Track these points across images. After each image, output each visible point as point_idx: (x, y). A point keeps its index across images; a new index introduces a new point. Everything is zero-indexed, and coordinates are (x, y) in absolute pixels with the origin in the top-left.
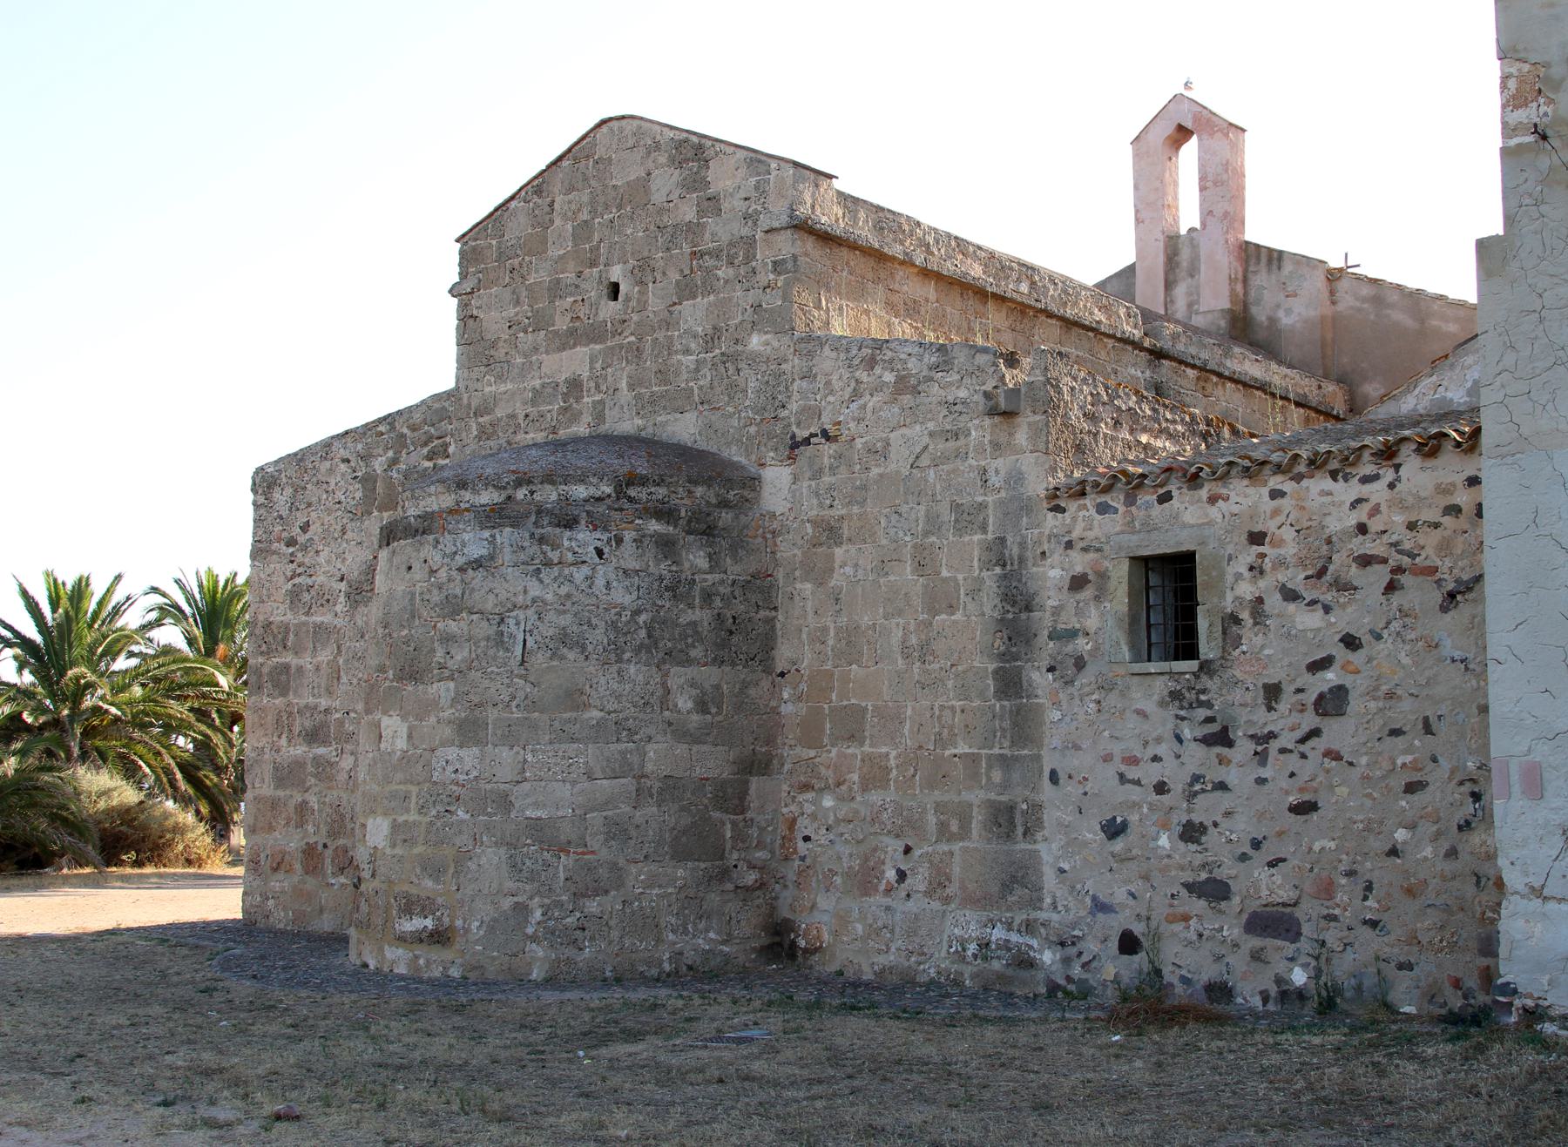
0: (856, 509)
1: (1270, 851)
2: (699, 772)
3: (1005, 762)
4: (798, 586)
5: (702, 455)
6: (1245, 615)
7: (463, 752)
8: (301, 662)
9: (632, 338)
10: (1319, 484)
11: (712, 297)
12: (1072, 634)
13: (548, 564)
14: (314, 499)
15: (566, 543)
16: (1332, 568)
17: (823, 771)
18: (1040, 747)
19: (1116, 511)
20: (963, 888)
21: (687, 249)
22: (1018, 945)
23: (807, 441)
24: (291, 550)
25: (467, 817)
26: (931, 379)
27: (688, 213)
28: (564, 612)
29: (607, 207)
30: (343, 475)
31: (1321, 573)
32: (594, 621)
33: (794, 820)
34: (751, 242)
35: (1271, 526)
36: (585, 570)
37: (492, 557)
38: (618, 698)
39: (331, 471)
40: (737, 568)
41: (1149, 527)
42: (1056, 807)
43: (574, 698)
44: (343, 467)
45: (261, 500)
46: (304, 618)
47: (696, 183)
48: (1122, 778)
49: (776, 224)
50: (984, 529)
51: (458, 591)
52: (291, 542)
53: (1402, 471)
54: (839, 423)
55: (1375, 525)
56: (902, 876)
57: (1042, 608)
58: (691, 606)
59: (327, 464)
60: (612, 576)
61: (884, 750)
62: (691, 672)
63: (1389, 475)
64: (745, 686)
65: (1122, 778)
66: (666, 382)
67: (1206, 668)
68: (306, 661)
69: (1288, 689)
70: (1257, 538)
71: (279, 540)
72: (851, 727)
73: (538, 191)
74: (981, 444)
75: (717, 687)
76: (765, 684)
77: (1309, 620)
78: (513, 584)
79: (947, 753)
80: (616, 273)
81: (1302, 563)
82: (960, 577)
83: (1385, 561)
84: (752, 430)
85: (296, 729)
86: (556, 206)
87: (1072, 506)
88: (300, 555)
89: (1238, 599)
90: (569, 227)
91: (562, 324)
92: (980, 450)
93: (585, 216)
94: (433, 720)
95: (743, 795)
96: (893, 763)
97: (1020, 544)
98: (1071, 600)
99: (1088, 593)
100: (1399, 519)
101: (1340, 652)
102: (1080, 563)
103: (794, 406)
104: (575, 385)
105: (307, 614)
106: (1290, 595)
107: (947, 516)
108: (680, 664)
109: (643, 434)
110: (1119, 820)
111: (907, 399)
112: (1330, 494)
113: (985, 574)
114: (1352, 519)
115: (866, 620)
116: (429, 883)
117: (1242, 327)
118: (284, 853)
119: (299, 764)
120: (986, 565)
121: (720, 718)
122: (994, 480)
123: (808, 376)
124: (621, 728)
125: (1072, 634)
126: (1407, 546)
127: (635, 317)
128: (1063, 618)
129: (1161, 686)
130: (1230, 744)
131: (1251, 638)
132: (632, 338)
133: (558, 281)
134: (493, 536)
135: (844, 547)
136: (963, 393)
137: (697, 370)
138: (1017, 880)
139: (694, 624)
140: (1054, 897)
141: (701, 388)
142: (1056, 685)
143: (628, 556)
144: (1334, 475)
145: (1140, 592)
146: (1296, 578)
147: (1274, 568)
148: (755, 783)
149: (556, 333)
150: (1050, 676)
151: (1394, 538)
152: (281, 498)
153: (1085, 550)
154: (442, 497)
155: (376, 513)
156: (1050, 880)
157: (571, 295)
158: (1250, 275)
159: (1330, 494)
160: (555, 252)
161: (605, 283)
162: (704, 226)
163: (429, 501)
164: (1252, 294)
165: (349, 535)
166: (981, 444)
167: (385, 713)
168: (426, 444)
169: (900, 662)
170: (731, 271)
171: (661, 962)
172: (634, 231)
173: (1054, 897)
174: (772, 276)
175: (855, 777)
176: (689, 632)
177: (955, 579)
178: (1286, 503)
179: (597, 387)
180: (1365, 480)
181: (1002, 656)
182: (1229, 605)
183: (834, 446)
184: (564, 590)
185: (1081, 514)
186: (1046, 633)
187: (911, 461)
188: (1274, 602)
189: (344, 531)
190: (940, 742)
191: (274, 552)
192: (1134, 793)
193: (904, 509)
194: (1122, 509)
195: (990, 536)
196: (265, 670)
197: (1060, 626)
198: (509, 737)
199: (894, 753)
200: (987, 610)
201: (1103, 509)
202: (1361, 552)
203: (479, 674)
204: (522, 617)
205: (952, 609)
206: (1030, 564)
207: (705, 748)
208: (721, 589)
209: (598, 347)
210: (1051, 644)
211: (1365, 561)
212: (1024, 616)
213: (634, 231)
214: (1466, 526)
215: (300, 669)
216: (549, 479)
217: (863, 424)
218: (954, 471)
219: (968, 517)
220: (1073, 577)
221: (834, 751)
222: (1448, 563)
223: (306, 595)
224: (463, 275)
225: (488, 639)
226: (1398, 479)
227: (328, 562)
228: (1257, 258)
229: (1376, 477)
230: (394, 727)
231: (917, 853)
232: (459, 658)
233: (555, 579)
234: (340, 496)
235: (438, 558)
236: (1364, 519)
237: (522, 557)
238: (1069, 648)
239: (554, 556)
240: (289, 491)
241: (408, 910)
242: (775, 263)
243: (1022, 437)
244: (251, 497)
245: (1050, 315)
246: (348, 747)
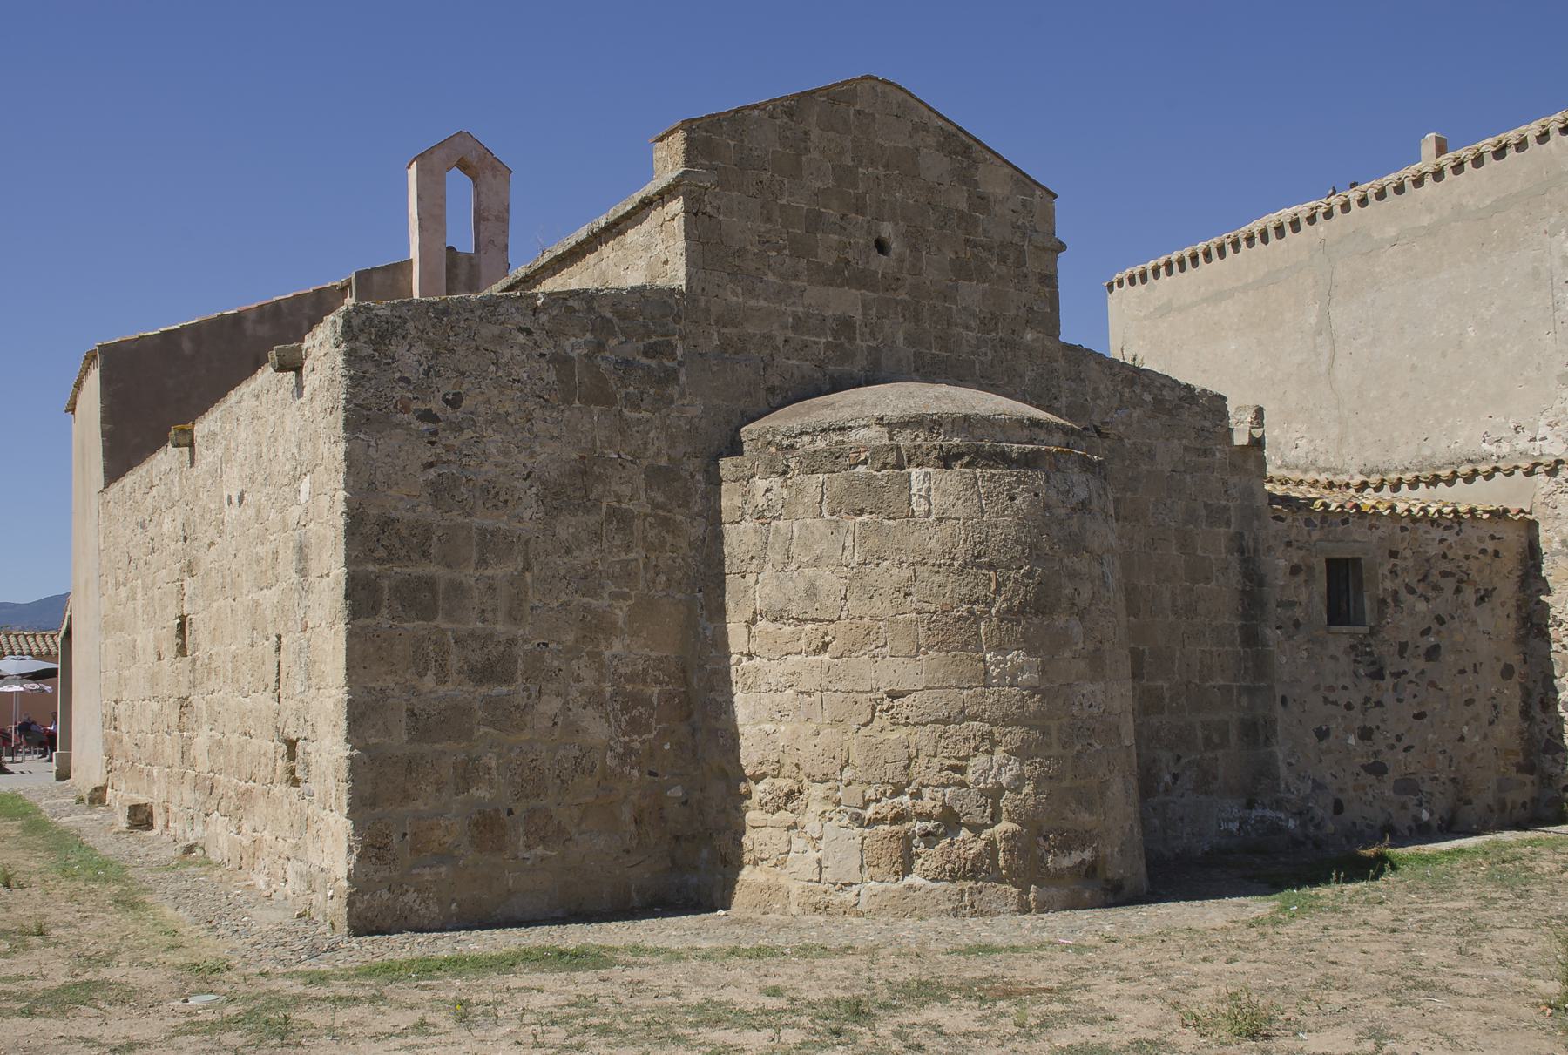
1: (1406, 741)
47: (965, 178)
48: (1326, 701)
50: (1228, 524)
56: (1175, 777)
65: (1326, 701)
69: (1411, 646)
73: (790, 112)
77: (1421, 606)
80: (887, 230)
83: (1453, 575)
99: (1301, 578)
101: (1435, 626)
106: (1412, 591)
116: (1086, 816)
129: (1345, 642)
130: (1383, 678)
141: (982, 363)
146: (1412, 579)
149: (820, 266)
156: (1283, 770)
188: (1403, 594)
191: (398, 426)
195: (1232, 530)
205: (1208, 580)
211: (1445, 574)
215: (457, 588)
231: (1184, 761)
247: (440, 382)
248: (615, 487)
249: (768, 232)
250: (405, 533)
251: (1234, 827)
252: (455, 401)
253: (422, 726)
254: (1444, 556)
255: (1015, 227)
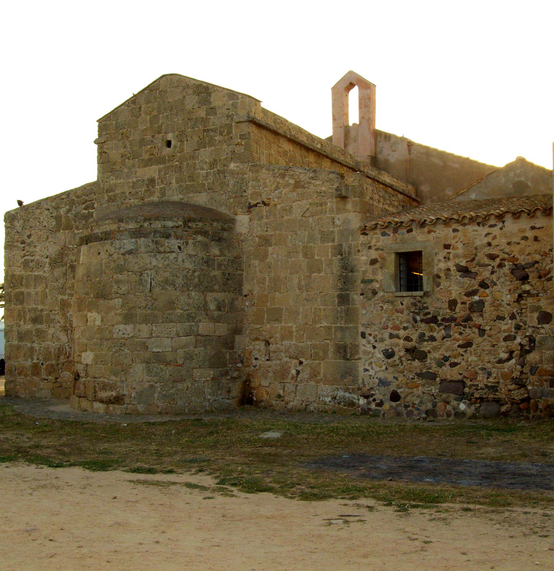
0: (278, 232)
2: (217, 333)
3: (342, 329)
4: (253, 262)
5: (211, 210)
6: (442, 275)
7: (127, 326)
8: (29, 290)
9: (177, 163)
10: (471, 228)
11: (213, 148)
12: (371, 281)
13: (160, 252)
14: (34, 225)
15: (166, 244)
16: (477, 258)
17: (264, 333)
18: (357, 323)
19: (389, 235)
20: (325, 376)
21: (201, 128)
22: (349, 398)
23: (256, 205)
24: (23, 245)
25: (129, 352)
26: (310, 183)
27: (202, 113)
28: (167, 271)
29: (165, 110)
30: (46, 215)
31: (473, 260)
32: (178, 275)
33: (251, 352)
34: (230, 126)
35: (453, 242)
36: (174, 255)
37: (137, 249)
38: (189, 305)
39: (41, 213)
40: (230, 255)
41: (403, 241)
42: (364, 345)
43: (171, 305)
44: (46, 212)
45: (9, 225)
46: (30, 273)
49: (242, 120)
50: (333, 241)
51: (122, 263)
52: (23, 242)
53: (505, 224)
54: (270, 199)
55: (494, 243)
56: (298, 372)
57: (358, 271)
58: (214, 269)
59: (39, 211)
60: (185, 257)
61: (291, 325)
62: (215, 295)
63: (500, 225)
64: (233, 300)
66: (194, 181)
67: (426, 294)
68: (32, 290)
70: (447, 247)
71: (17, 242)
72: (276, 315)
74: (332, 208)
75: (224, 301)
76: (240, 299)
78: (146, 260)
79: (317, 326)
80: (170, 137)
81: (465, 256)
82: (323, 259)
84: (232, 200)
85: (28, 317)
86: (142, 109)
87: (371, 233)
88: (27, 248)
89: (440, 270)
90: (148, 117)
91: (146, 157)
92: (332, 210)
93: (155, 113)
94: (113, 314)
95: (233, 342)
96: (294, 329)
97: (349, 247)
98: (370, 268)
99: (377, 265)
100: (504, 241)
102: (374, 254)
103: (249, 192)
104: (152, 181)
105: (32, 271)
107: (318, 236)
108: (210, 291)
109: (183, 201)
110: (390, 350)
111: (300, 190)
112: (477, 231)
113: (334, 258)
114: (486, 240)
115: (282, 275)
117: (375, 161)
118: (23, 367)
119: (28, 332)
120: (334, 255)
121: (224, 313)
122: (338, 222)
123: (256, 179)
124: (190, 318)
125: (371, 281)
126: (507, 250)
127: (179, 155)
128: (367, 275)
131: (444, 283)
132: (177, 163)
133: (144, 139)
134: (137, 241)
135: (272, 247)
136: (324, 189)
137: (207, 176)
138: (349, 373)
139: (214, 276)
140: (363, 380)
141: (208, 183)
142: (364, 300)
143: (190, 249)
144: (479, 224)
145: (398, 265)
147: (454, 257)
148: (237, 338)
149: (143, 160)
150: (362, 297)
151: (503, 247)
152: (18, 225)
153: (377, 249)
154: (111, 225)
155: (62, 231)
157: (149, 145)
158: (378, 142)
159: (477, 231)
160: (142, 127)
161: (165, 140)
162: (209, 119)
163: (105, 227)
164: (378, 150)
165: (50, 239)
166: (332, 208)
167: (90, 311)
168: (84, 203)
169: (297, 291)
170: (221, 137)
171: (206, 406)
172: (178, 120)
173: (363, 380)
174: (239, 140)
175: (278, 335)
176: (214, 279)
177: (321, 261)
178: (459, 234)
179: (162, 181)
180: (491, 226)
181: (341, 289)
182: (435, 271)
183: (268, 208)
184: (166, 263)
185: (375, 236)
186: (360, 280)
187: (302, 214)
189: (48, 238)
190: (315, 322)
191: (16, 246)
192: (396, 340)
193: (299, 232)
194: (392, 235)
195: (336, 244)
196: (12, 294)
197: (366, 278)
198: (146, 320)
199: (295, 326)
200: (335, 272)
201: (384, 234)
202: (489, 253)
203: (132, 296)
204: (149, 273)
205: (319, 271)
206: (353, 255)
207: (220, 324)
208: (224, 263)
209: (162, 166)
210: (362, 285)
212: (350, 274)
213: (178, 120)
214: (529, 244)
215: (29, 294)
216: (157, 219)
217: (280, 199)
218: (320, 218)
219: (326, 237)
220: (371, 260)
221: (268, 326)
222: (522, 257)
223: (31, 263)
224: (100, 135)
225: (136, 282)
226: (504, 226)
227: (41, 250)
228: (377, 134)
229: (495, 225)
230: (95, 318)
232: (124, 289)
233: (163, 258)
234: (45, 223)
235: (113, 250)
236: (490, 240)
237: (149, 250)
238: (370, 286)
239: (162, 249)
240: (21, 222)
241: (104, 387)
242: (241, 135)
243: (349, 206)
244: (4, 224)
245: (327, 157)
246: (51, 325)
247: (26, 231)
248: (70, 257)
249: (125, 151)
250: (17, 278)
251: (328, 399)
252: (29, 236)
253: (21, 337)
254: (489, 244)
255: (228, 116)
